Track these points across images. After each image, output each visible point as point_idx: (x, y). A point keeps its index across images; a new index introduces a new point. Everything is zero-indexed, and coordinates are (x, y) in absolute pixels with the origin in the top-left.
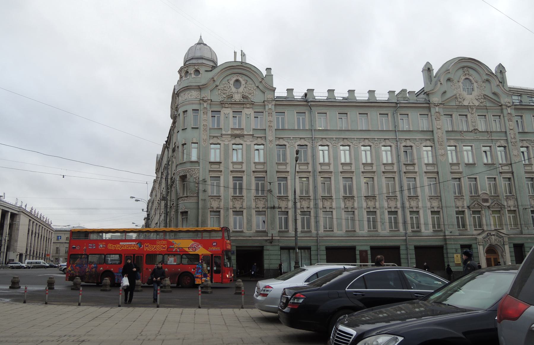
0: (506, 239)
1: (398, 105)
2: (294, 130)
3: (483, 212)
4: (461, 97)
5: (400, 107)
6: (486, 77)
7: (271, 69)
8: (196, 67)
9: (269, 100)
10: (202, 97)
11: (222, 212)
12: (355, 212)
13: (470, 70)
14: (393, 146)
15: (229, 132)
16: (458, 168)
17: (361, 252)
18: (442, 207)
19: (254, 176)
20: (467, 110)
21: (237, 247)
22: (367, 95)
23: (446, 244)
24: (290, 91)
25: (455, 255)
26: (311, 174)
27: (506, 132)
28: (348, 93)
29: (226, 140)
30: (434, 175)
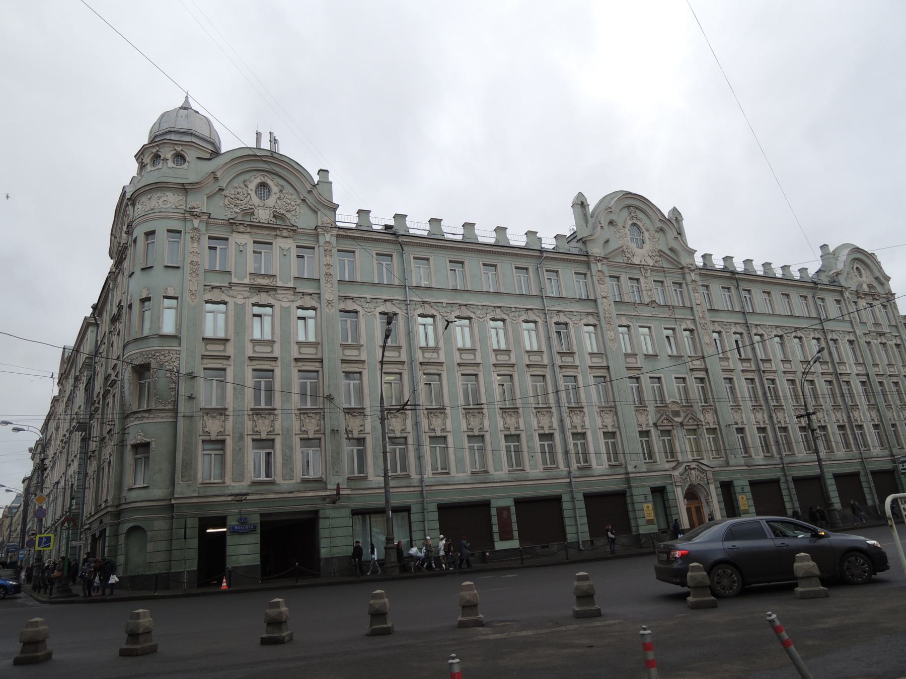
0: (710, 475)
2: (372, 284)
4: (629, 251)
8: (179, 149)
10: (189, 206)
13: (637, 211)
15: (247, 281)
17: (500, 510)
20: (638, 271)
21: (262, 515)
23: (630, 487)
24: (803, 270)
25: (645, 505)
28: (357, 215)
29: (239, 296)
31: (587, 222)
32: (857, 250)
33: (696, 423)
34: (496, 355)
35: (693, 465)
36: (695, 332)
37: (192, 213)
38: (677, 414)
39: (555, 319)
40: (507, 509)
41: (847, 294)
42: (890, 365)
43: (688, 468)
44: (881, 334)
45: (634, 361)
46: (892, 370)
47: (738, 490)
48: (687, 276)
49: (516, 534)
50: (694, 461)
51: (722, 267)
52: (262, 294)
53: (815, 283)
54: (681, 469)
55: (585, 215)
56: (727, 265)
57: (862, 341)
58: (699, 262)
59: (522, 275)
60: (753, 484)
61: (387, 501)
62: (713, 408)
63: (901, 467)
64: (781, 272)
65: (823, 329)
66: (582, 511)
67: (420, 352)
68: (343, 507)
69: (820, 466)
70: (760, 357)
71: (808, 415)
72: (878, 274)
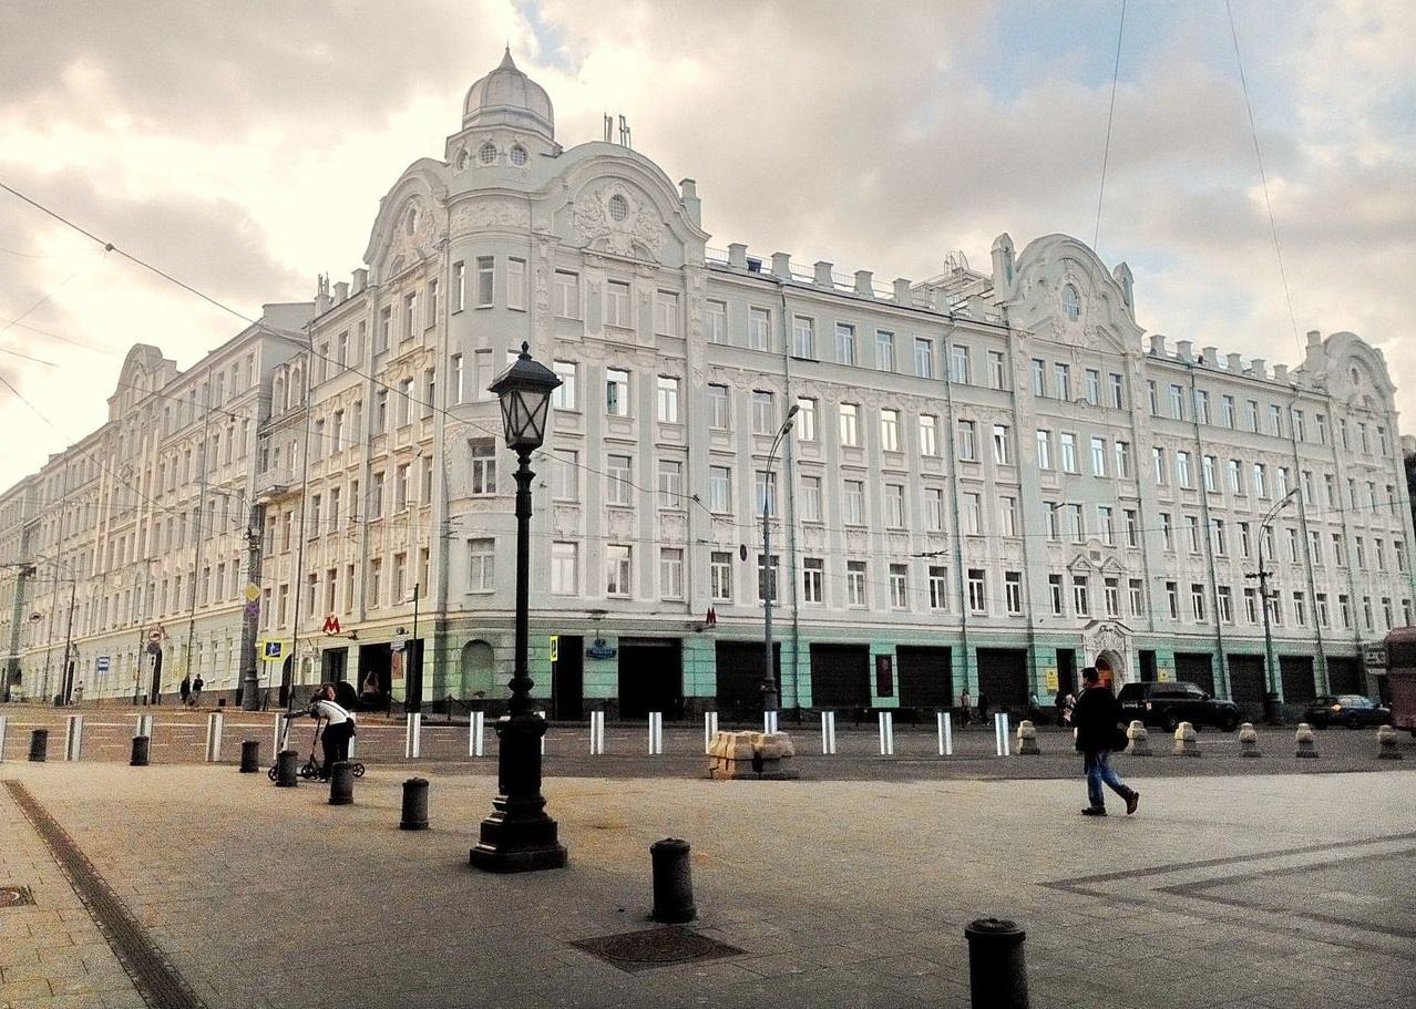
0: (1129, 641)
1: (956, 324)
2: (746, 350)
3: (1092, 579)
4: (1060, 325)
5: (1301, 398)
6: (1102, 288)
7: (1319, 333)
8: (520, 139)
9: (695, 264)
10: (535, 225)
11: (583, 545)
12: (633, 549)
13: (1076, 266)
14: (942, 416)
15: (601, 336)
16: (727, 443)
17: (879, 658)
18: (689, 541)
19: (843, 478)
20: (1068, 355)
21: (621, 639)
22: (892, 289)
23: (1032, 646)
24: (1233, 357)
25: (1048, 670)
26: (946, 482)
27: (1012, 393)
28: (728, 249)
29: (644, 364)
30: (679, 456)
31: (1010, 277)
32: (1359, 343)
33: (1118, 571)
34: (661, 430)
35: (1111, 626)
36: (1131, 446)
37: (538, 237)
38: (1096, 555)
39: (961, 415)
40: (889, 658)
41: (1334, 408)
42: (1241, 496)
43: (1104, 629)
44: (1370, 470)
45: (899, 462)
46: (1377, 521)
47: (1159, 663)
48: (1131, 367)
49: (896, 691)
50: (1111, 620)
51: (1175, 356)
52: (620, 354)
53: (1294, 389)
54: (1096, 629)
55: (1009, 268)
56: (1181, 352)
57: (1343, 479)
58: (1271, 374)
59: (761, 319)
60: (1179, 657)
61: (768, 633)
62: (1142, 552)
63: (1368, 657)
64: (1273, 374)
65: (1295, 456)
66: (805, 669)
67: (658, 428)
68: (706, 637)
69: (1268, 643)
70: (1207, 489)
71: (1263, 575)
72: (1379, 381)
